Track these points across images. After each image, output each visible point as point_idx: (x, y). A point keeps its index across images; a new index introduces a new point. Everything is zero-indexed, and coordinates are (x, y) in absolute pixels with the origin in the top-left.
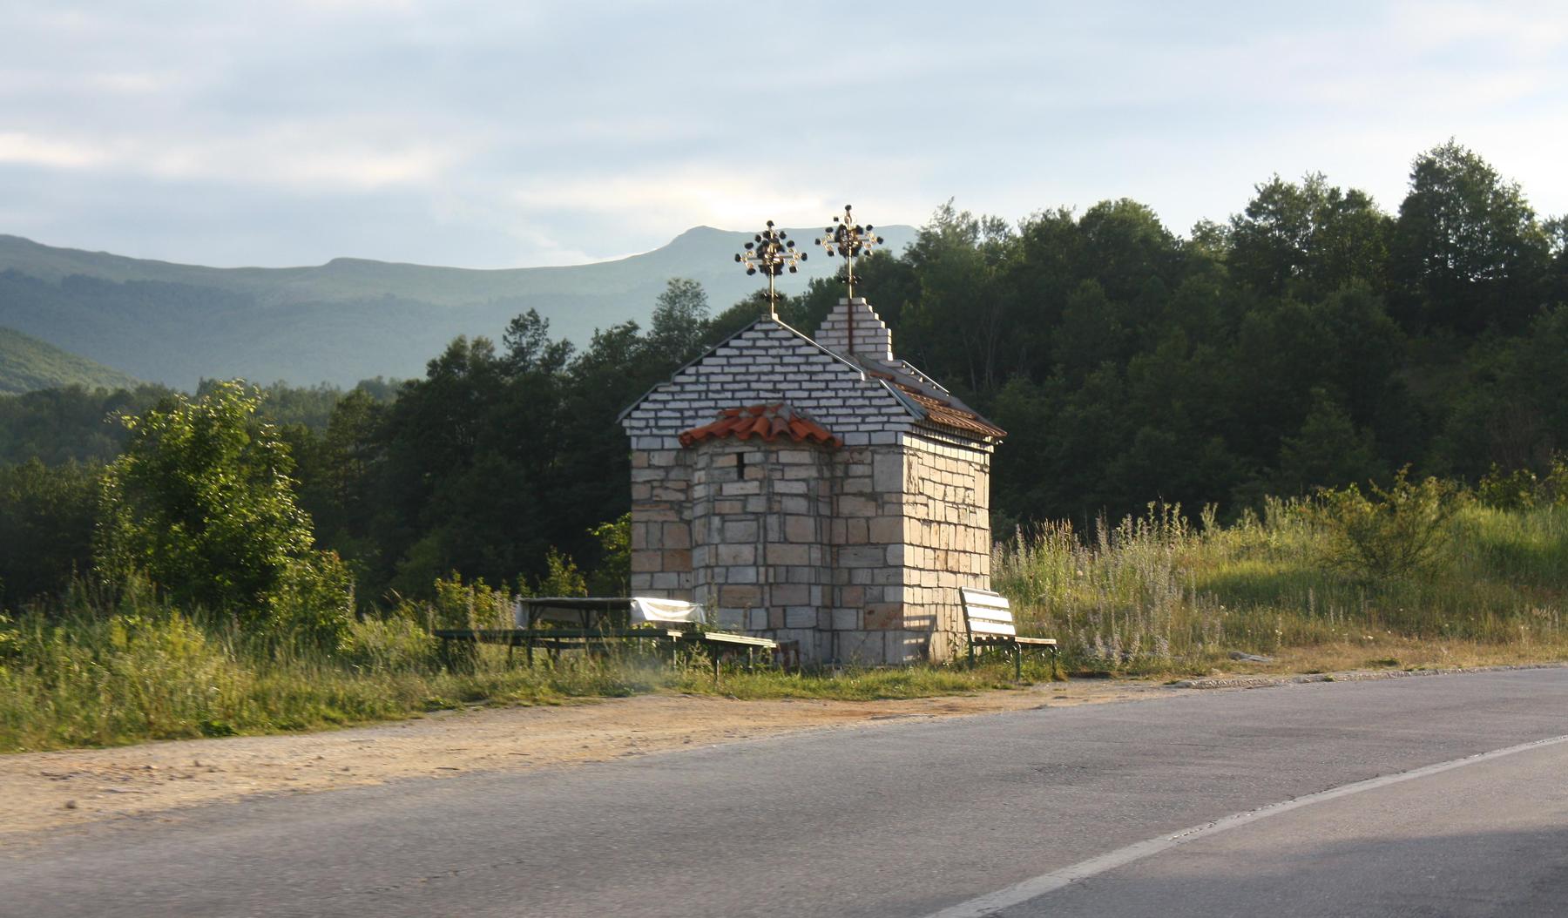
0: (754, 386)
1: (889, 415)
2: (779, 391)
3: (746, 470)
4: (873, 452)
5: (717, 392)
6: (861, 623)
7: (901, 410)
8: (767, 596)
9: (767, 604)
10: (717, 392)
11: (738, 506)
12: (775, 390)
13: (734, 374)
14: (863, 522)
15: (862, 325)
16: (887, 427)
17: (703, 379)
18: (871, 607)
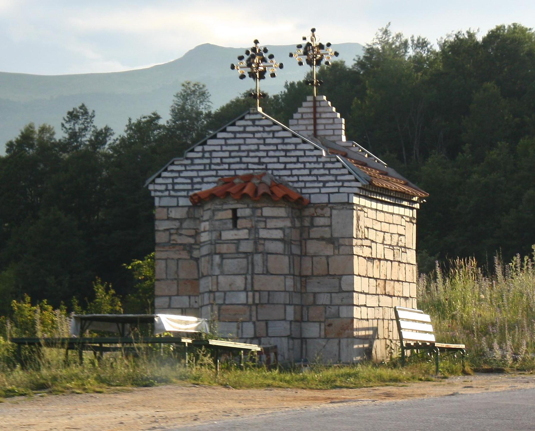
4: (332, 208)
6: (323, 333)
7: (352, 177)
8: (254, 313)
9: (254, 319)
12: (260, 163)
14: (324, 259)
15: (324, 116)
16: (342, 190)
18: (330, 321)
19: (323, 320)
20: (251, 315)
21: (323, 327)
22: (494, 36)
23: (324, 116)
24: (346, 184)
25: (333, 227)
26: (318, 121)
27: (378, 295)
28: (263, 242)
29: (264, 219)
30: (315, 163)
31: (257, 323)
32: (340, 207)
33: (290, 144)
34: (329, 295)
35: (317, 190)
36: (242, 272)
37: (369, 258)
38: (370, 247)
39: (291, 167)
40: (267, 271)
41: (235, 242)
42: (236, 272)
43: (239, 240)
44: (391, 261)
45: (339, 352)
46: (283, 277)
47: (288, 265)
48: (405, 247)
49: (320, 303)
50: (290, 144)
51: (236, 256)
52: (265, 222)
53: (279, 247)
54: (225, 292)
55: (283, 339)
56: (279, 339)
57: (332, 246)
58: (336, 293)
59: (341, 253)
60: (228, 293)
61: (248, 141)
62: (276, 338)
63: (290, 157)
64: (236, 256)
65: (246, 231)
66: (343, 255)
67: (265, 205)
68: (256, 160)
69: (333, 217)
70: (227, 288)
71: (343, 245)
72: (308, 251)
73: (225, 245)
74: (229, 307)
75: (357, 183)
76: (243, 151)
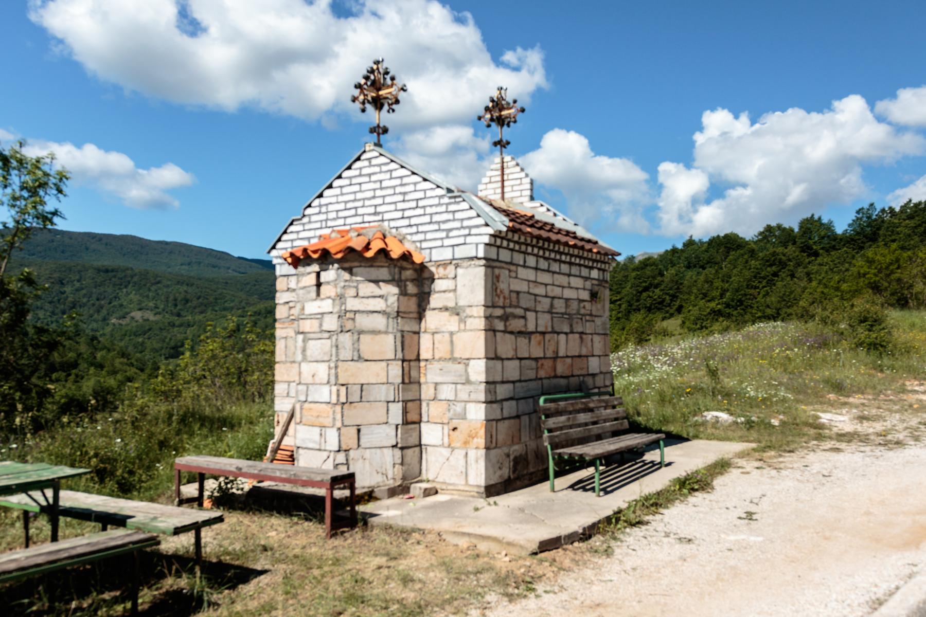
0: (360, 211)
1: (470, 228)
2: (379, 213)
3: (322, 288)
4: (457, 266)
5: (334, 219)
6: (446, 440)
7: (480, 221)
8: (339, 416)
9: (339, 424)
10: (334, 219)
11: (316, 323)
12: (375, 214)
13: (346, 202)
14: (447, 336)
15: (511, 177)
16: (469, 239)
17: (324, 209)
18: (455, 423)
19: (446, 421)
20: (334, 419)
21: (446, 431)
22: (726, 236)
23: (511, 177)
24: (474, 231)
25: (458, 292)
26: (506, 183)
27: (541, 379)
28: (352, 315)
29: (355, 284)
30: (436, 205)
31: (343, 430)
32: (466, 264)
33: (408, 184)
34: (454, 386)
35: (439, 243)
36: (326, 358)
37: (520, 333)
38: (524, 317)
39: (396, 213)
40: (359, 357)
41: (319, 316)
42: (319, 358)
43: (323, 314)
44: (566, 334)
45: (466, 469)
46: (384, 364)
47: (393, 348)
48: (591, 315)
49: (443, 398)
50: (408, 184)
51: (319, 335)
52: (357, 288)
53: (379, 322)
54: (307, 384)
55: (385, 450)
56: (378, 450)
57: (457, 318)
58: (463, 384)
59: (467, 328)
60: (310, 386)
61: (364, 187)
62: (373, 450)
63: (408, 201)
64: (319, 335)
65: (330, 301)
66: (471, 330)
67: (356, 264)
68: (372, 210)
69: (458, 278)
70: (310, 380)
71: (470, 317)
72: (428, 326)
73: (308, 322)
74: (312, 405)
75: (488, 228)
76: (359, 200)
